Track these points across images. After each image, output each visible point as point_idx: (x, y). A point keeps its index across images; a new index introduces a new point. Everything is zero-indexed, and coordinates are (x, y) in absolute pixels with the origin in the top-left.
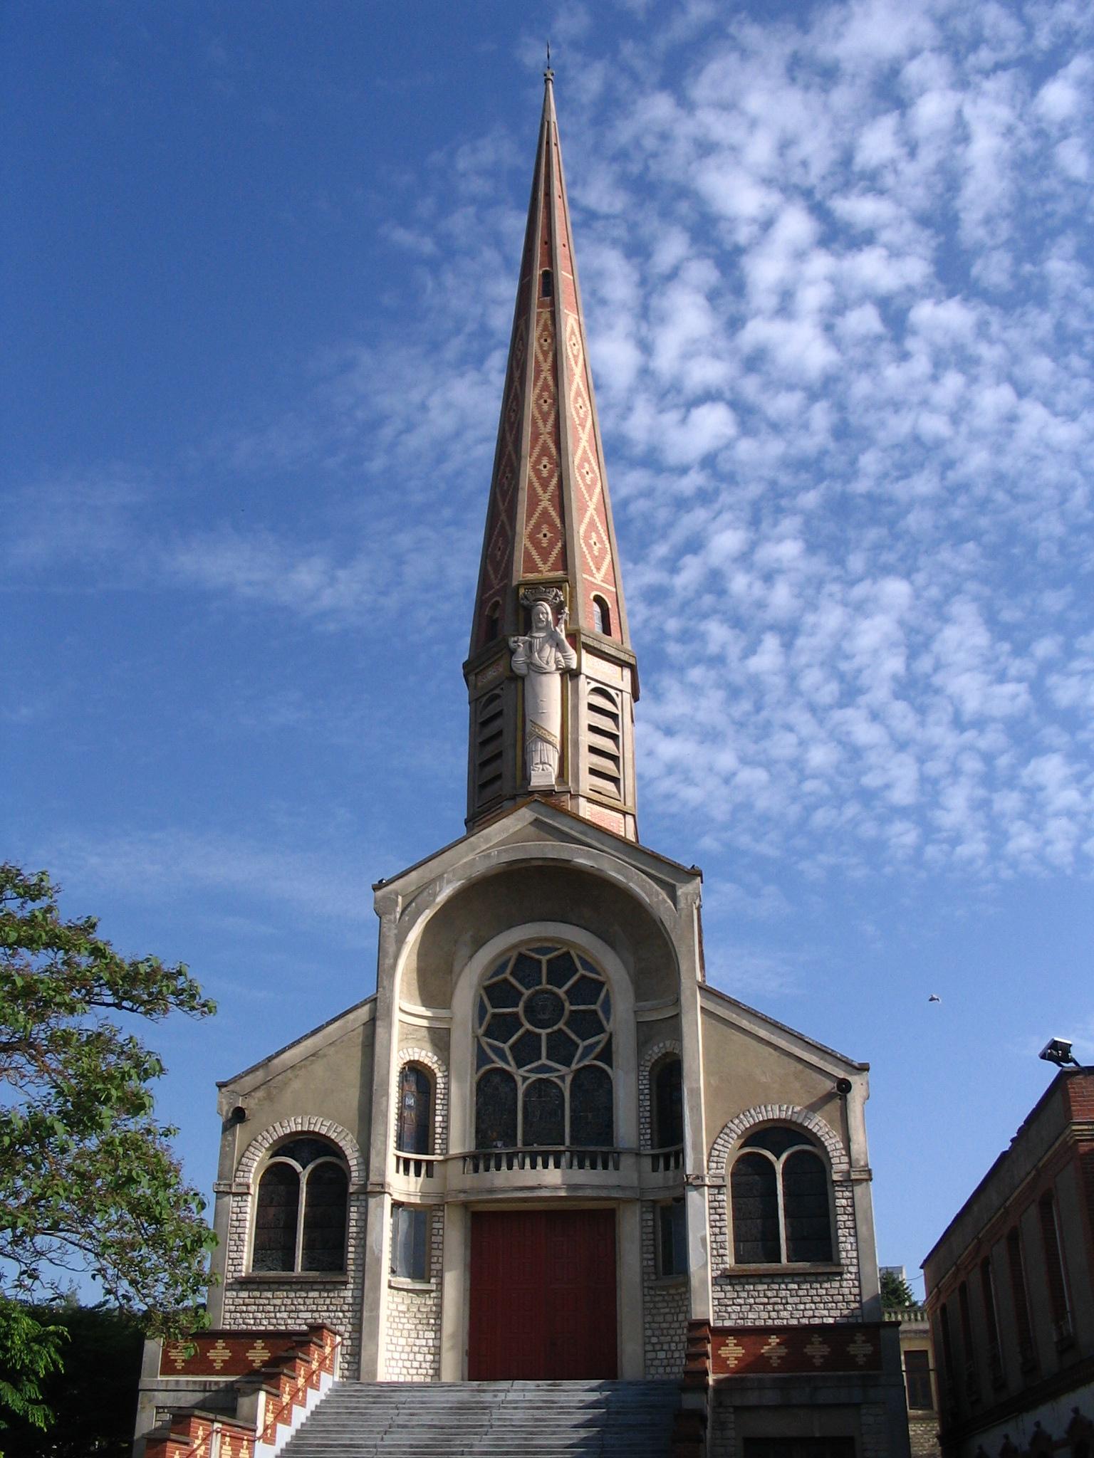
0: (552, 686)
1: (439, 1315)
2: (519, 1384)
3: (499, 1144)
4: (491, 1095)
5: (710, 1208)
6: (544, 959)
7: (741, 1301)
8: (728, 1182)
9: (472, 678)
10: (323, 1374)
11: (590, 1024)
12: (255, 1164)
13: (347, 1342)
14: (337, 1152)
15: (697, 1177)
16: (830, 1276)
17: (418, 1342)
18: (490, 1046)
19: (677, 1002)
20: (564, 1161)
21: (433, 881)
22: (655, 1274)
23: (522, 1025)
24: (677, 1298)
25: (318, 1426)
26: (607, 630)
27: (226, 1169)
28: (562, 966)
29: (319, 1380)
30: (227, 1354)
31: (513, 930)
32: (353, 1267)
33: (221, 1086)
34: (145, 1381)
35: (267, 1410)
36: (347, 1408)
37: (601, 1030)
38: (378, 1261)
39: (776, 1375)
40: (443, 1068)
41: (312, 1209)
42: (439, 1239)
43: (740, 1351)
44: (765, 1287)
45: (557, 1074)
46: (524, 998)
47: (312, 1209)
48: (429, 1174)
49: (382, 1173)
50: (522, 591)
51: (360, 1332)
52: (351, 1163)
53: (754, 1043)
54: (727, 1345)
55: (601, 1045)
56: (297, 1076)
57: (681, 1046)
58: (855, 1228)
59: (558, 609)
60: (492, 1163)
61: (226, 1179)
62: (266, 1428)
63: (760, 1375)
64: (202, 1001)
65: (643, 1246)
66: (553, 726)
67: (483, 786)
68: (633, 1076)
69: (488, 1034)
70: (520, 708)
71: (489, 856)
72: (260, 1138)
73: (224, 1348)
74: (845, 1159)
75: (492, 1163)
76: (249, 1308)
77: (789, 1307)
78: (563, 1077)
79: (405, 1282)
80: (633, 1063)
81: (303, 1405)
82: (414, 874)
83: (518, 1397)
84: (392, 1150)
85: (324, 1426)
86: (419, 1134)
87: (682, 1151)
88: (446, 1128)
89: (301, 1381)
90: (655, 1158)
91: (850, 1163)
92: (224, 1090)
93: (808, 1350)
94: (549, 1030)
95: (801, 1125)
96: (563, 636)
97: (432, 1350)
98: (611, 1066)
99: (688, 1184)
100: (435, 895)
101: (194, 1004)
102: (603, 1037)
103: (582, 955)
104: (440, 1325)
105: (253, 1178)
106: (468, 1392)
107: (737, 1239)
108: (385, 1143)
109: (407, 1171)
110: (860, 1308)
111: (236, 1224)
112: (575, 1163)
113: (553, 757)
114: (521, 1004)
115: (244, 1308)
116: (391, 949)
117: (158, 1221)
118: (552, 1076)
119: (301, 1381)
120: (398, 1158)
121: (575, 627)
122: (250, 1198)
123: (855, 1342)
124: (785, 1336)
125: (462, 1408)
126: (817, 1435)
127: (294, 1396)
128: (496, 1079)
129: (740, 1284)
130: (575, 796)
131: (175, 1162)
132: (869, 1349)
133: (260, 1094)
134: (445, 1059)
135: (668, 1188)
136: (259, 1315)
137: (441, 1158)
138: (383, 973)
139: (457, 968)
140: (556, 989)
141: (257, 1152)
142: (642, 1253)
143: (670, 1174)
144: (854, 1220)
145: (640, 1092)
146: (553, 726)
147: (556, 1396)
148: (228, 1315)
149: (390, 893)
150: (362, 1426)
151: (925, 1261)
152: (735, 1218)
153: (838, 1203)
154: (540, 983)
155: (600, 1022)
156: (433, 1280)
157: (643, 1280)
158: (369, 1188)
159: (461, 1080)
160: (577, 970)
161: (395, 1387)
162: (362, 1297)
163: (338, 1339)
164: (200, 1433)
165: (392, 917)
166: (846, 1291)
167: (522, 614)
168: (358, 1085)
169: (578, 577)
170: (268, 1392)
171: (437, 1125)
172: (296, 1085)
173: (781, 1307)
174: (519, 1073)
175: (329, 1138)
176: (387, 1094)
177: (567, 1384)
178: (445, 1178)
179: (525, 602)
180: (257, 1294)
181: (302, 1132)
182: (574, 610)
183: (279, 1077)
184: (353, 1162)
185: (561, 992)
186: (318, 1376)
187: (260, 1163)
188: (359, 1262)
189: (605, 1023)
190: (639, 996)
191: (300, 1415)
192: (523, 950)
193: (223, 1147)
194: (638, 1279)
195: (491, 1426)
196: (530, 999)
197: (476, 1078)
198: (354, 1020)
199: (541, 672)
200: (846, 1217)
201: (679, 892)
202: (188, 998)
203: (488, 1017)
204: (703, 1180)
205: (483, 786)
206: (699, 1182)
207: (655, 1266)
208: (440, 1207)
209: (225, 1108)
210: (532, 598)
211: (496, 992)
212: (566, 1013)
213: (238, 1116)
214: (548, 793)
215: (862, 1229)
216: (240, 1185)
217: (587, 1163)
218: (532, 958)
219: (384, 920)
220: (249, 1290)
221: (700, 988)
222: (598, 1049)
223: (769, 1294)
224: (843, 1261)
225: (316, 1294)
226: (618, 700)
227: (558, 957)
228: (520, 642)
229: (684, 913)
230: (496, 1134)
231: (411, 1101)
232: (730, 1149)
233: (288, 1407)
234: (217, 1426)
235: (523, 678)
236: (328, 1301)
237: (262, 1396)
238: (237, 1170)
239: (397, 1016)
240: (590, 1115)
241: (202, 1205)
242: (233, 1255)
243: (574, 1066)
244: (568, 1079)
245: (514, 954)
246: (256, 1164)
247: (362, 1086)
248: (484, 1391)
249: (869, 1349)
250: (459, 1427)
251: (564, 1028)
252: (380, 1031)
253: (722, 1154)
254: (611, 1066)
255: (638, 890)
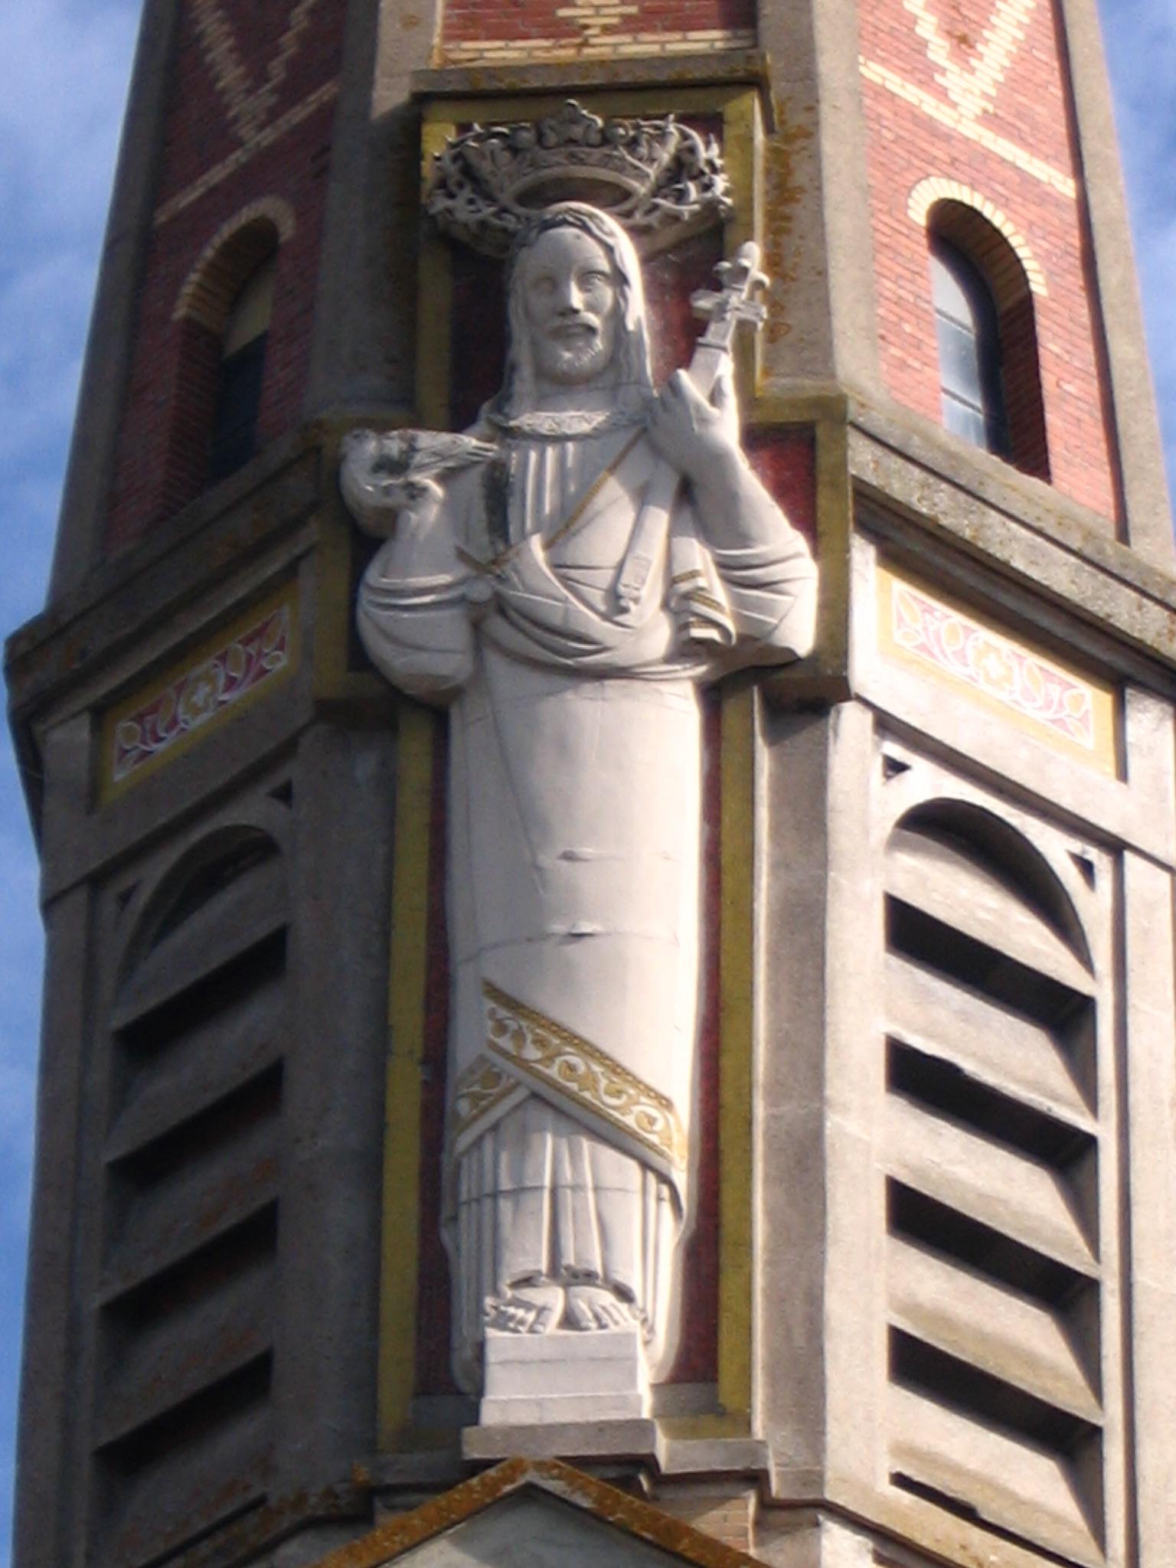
0: (640, 767)
9: (68, 737)
26: (1016, 426)
50: (438, 138)
59: (691, 260)
66: (648, 1024)
67: (131, 1456)
70: (411, 899)
96: (727, 427)
113: (647, 1245)
121: (810, 386)
146: (648, 1024)
167: (437, 291)
169: (830, 65)
179: (465, 210)
182: (799, 274)
199: (571, 662)
205: (131, 1456)
210: (508, 178)
214: (612, 1483)
226: (1092, 907)
228: (420, 477)
235: (435, 711)
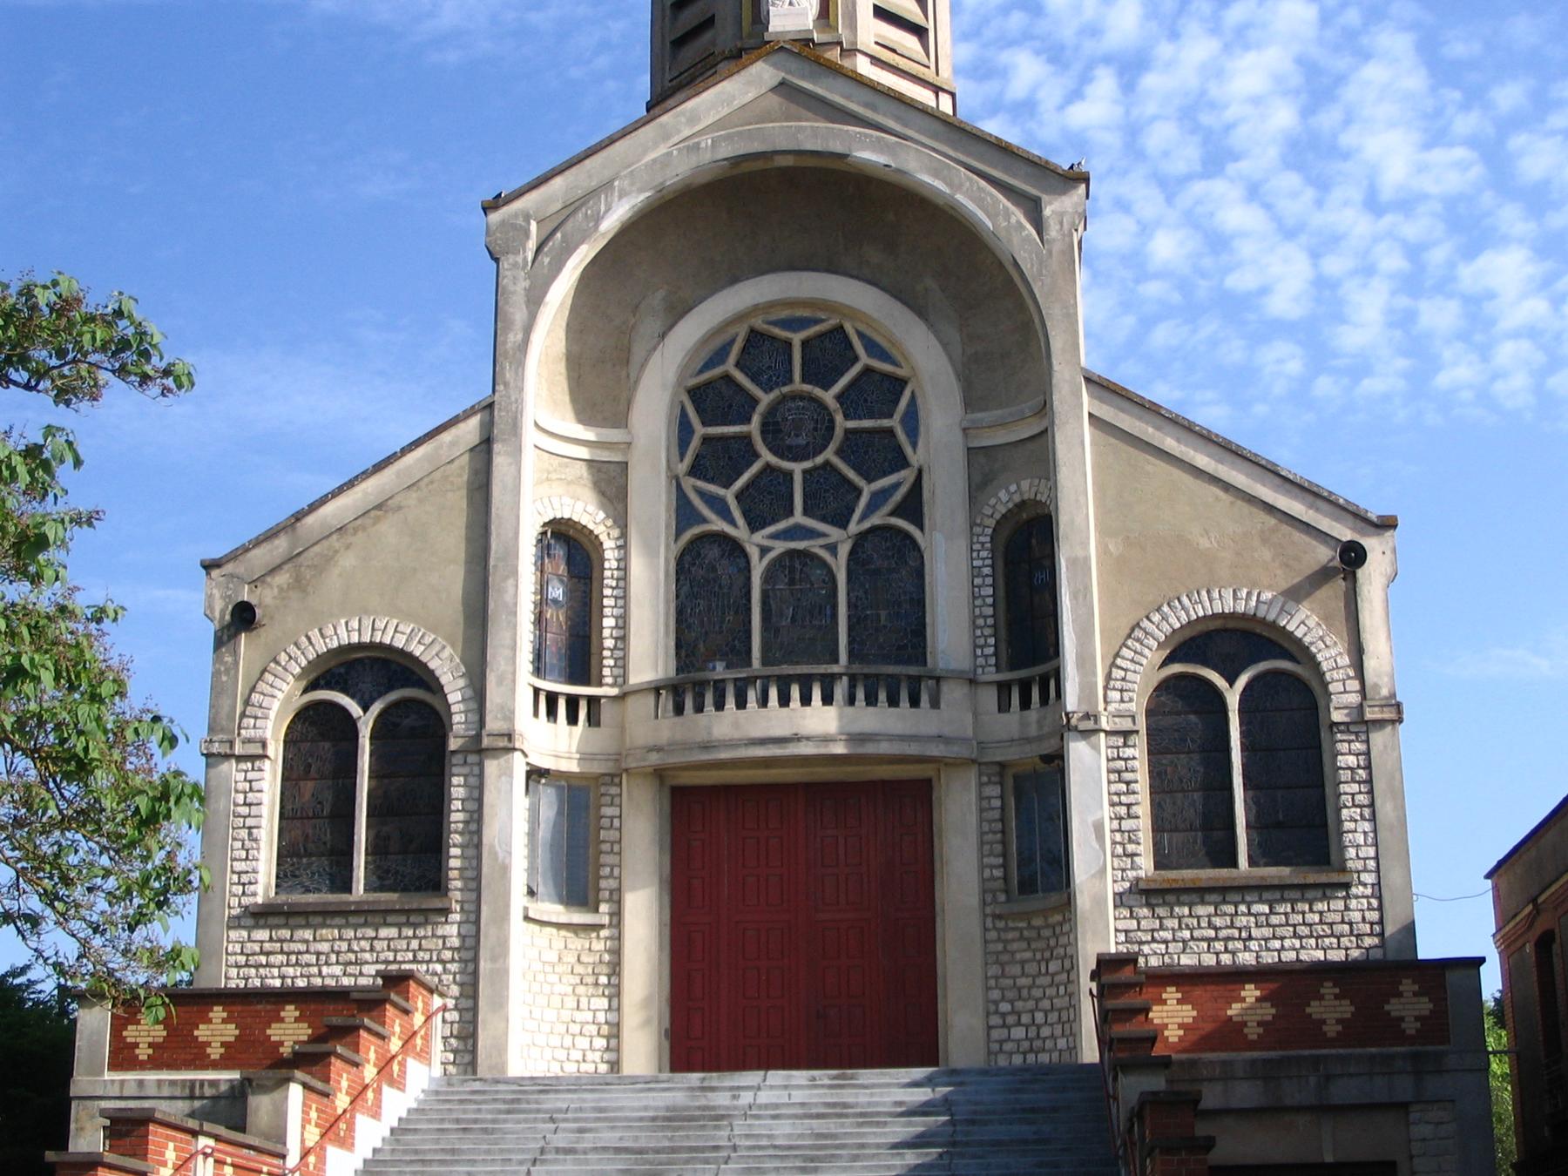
1: (616, 968)
2: (776, 1077)
3: (720, 666)
4: (703, 577)
5: (1109, 771)
6: (797, 338)
7: (1168, 935)
8: (1142, 724)
10: (412, 1064)
11: (879, 453)
12: (276, 705)
13: (455, 1016)
14: (430, 682)
15: (1087, 716)
16: (1325, 890)
17: (579, 1016)
18: (701, 494)
19: (1044, 408)
20: (840, 691)
21: (593, 193)
22: (1007, 892)
23: (757, 456)
24: (1046, 933)
25: (405, 1152)
27: (225, 710)
28: (830, 350)
29: (403, 1072)
30: (231, 1032)
31: (737, 287)
32: (458, 884)
33: (209, 566)
34: (81, 1083)
35: (305, 1121)
36: (458, 1121)
37: (901, 462)
38: (505, 870)
39: (1255, 1054)
40: (616, 533)
41: (381, 780)
42: (613, 835)
43: (1188, 1013)
44: (1211, 909)
45: (822, 541)
46: (761, 408)
47: (381, 780)
48: (593, 720)
49: (510, 716)
51: (475, 997)
52: (451, 698)
53: (1187, 479)
54: (1164, 1002)
55: (903, 490)
56: (348, 547)
57: (1053, 488)
58: (1372, 805)
60: (709, 698)
61: (222, 730)
62: (305, 1154)
63: (1223, 1056)
64: (163, 365)
65: (982, 843)
67: (679, 43)
68: (962, 544)
69: (694, 471)
71: (697, 146)
72: (283, 658)
73: (224, 1021)
74: (1354, 685)
75: (709, 698)
76: (272, 959)
77: (1254, 945)
78: (835, 546)
79: (555, 911)
80: (961, 519)
81: (376, 1114)
82: (558, 182)
83: (778, 1098)
84: (525, 679)
85: (416, 1152)
86: (576, 651)
87: (1057, 674)
88: (623, 640)
89: (370, 1072)
90: (1003, 688)
91: (1363, 691)
92: (215, 573)
93: (1314, 1009)
94: (807, 464)
95: (1273, 625)
97: (605, 1029)
98: (921, 528)
99: (1068, 727)
100: (598, 219)
101: (148, 369)
102: (906, 476)
103: (868, 332)
104: (618, 986)
105: (272, 727)
106: (684, 1089)
107: (1158, 828)
108: (513, 660)
109: (552, 713)
110: (1383, 945)
111: (244, 810)
112: (860, 695)
114: (756, 419)
115: (263, 959)
116: (519, 315)
117: (81, 768)
118: (814, 546)
119: (370, 1072)
120: (537, 691)
122: (267, 764)
123: (1400, 995)
124: (1273, 986)
125: (673, 1118)
126: (1329, 1159)
127: (357, 1097)
128: (713, 552)
129: (1165, 904)
130: (853, 51)
131: (114, 663)
132: (1425, 1006)
133: (282, 579)
134: (621, 521)
135: (1028, 740)
136: (290, 971)
137: (614, 691)
138: (503, 358)
139: (637, 356)
140: (818, 392)
141: (278, 683)
142: (982, 856)
143: (1033, 714)
144: (1371, 792)
145: (975, 572)
147: (847, 1096)
148: (233, 972)
149: (516, 215)
150: (488, 1152)
151: (1500, 864)
152: (1154, 790)
153: (1342, 761)
154: (791, 381)
155: (899, 450)
156: (604, 908)
157: (984, 903)
158: (486, 742)
159: (650, 552)
160: (856, 359)
161: (546, 1086)
162: (477, 936)
163: (437, 1002)
164: (170, 1155)
165: (520, 259)
166: (1356, 916)
168: (462, 556)
170: (305, 1086)
171: (606, 633)
172: (347, 561)
173: (1239, 945)
174: (752, 542)
175: (410, 656)
176: (514, 573)
177: (867, 1076)
178: (622, 729)
180: (286, 933)
181: (361, 646)
183: (317, 549)
184: (454, 697)
185: (829, 397)
186: (402, 1064)
187: (288, 698)
188: (470, 874)
189: (908, 450)
190: (969, 404)
191: (370, 1134)
192: (758, 323)
193: (216, 674)
194: (974, 901)
195: (735, 1148)
196: (773, 409)
197: (676, 549)
198: (453, 444)
200: (1355, 788)
201: (1047, 211)
202: (132, 355)
203: (695, 443)
204: (1096, 718)
205: (679, 43)
206: (1090, 725)
207: (1005, 878)
208: (613, 778)
209: (218, 605)
211: (709, 398)
212: (839, 433)
213: (243, 617)
214: (803, 49)
215: (1385, 809)
216: (249, 741)
217: (882, 696)
218: (773, 338)
219: (505, 264)
220: (271, 928)
221: (1088, 380)
222: (898, 496)
223: (1218, 921)
224: (1350, 864)
225: (393, 932)
227: (821, 336)
229: (1057, 248)
230: (711, 646)
231: (557, 592)
232: (1144, 669)
233: (348, 1116)
234: (203, 1142)
236: (415, 944)
237: (295, 1092)
238: (243, 715)
239: (530, 436)
240: (883, 614)
241: (171, 741)
242: (239, 866)
243: (854, 527)
244: (844, 550)
245: (742, 332)
246: (277, 706)
247: (470, 561)
248: (713, 1089)
249: (1425, 1006)
250: (673, 1150)
251: (836, 461)
252: (500, 461)
253: (1130, 676)
254: (921, 528)
255: (971, 206)
